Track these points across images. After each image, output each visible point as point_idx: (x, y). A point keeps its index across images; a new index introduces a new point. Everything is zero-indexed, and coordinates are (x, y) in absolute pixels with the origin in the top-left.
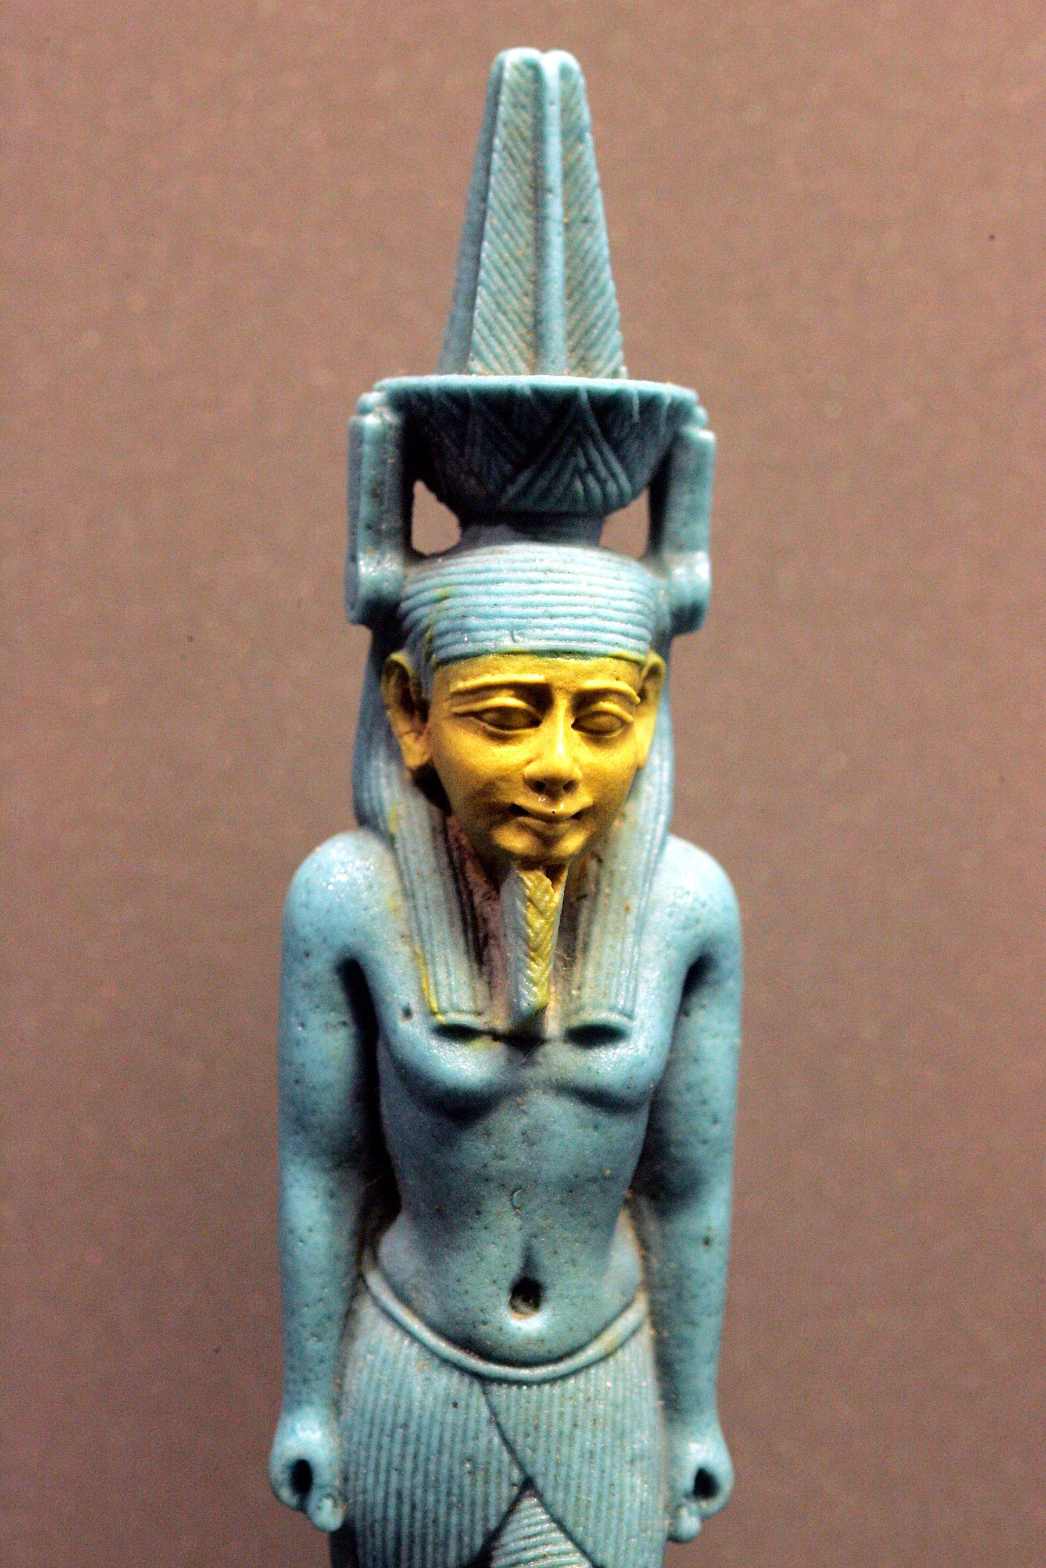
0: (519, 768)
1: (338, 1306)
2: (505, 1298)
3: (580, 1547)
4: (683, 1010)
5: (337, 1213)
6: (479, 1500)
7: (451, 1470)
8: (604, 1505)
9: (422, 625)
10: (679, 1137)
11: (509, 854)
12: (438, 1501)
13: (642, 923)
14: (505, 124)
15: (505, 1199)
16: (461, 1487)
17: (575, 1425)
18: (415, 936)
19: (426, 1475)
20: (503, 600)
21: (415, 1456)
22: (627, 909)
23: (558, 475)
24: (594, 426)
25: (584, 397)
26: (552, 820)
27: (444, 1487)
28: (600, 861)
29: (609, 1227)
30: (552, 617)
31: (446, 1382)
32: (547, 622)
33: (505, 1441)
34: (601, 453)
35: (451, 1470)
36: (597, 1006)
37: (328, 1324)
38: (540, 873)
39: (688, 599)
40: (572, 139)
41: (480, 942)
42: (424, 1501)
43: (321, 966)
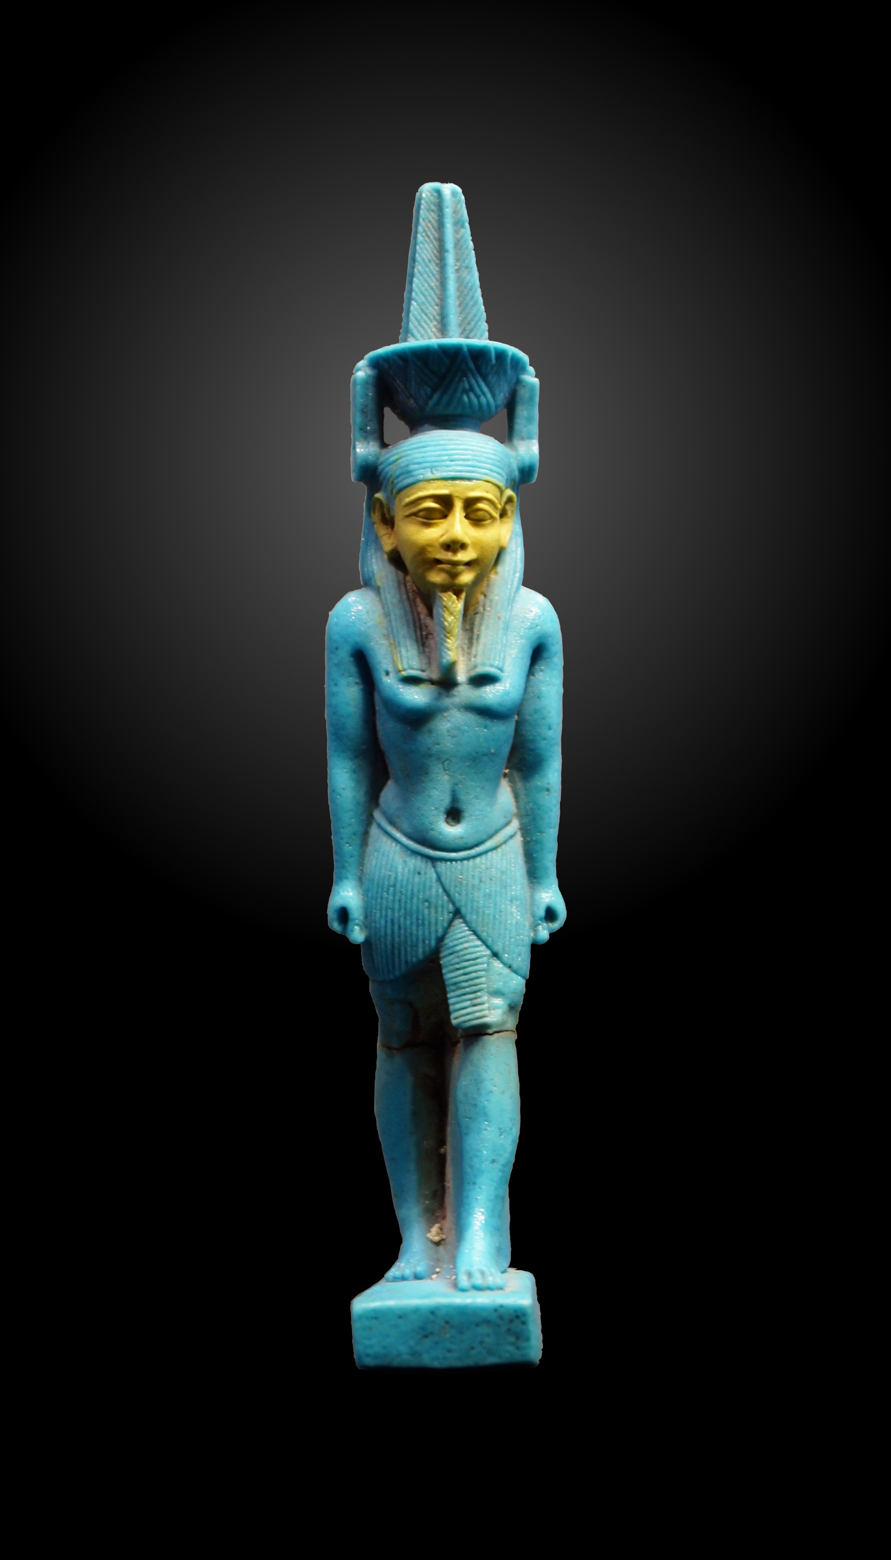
0: (437, 539)
1: (359, 829)
2: (443, 817)
3: (484, 943)
4: (531, 671)
5: (358, 781)
6: (433, 921)
7: (418, 907)
8: (497, 922)
9: (388, 475)
10: (531, 738)
11: (434, 585)
12: (412, 923)
13: (507, 628)
14: (424, 220)
15: (440, 766)
16: (423, 914)
17: (481, 881)
18: (390, 635)
19: (405, 909)
20: (427, 454)
21: (400, 901)
22: (499, 618)
23: (455, 392)
24: (472, 365)
25: (465, 349)
26: (455, 564)
27: (414, 916)
28: (485, 596)
29: (496, 786)
30: (452, 461)
31: (415, 863)
32: (448, 463)
33: (445, 890)
34: (477, 382)
35: (418, 907)
36: (483, 665)
37: (354, 838)
38: (450, 593)
39: (527, 463)
40: (459, 226)
41: (425, 636)
42: (405, 924)
43: (344, 654)
